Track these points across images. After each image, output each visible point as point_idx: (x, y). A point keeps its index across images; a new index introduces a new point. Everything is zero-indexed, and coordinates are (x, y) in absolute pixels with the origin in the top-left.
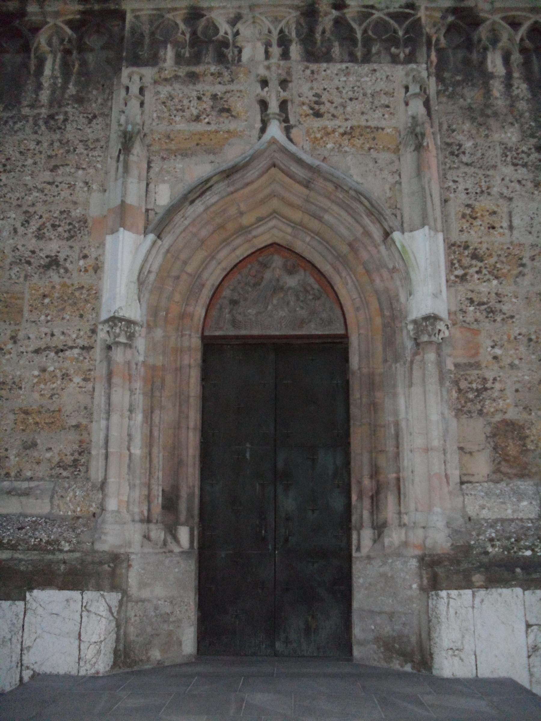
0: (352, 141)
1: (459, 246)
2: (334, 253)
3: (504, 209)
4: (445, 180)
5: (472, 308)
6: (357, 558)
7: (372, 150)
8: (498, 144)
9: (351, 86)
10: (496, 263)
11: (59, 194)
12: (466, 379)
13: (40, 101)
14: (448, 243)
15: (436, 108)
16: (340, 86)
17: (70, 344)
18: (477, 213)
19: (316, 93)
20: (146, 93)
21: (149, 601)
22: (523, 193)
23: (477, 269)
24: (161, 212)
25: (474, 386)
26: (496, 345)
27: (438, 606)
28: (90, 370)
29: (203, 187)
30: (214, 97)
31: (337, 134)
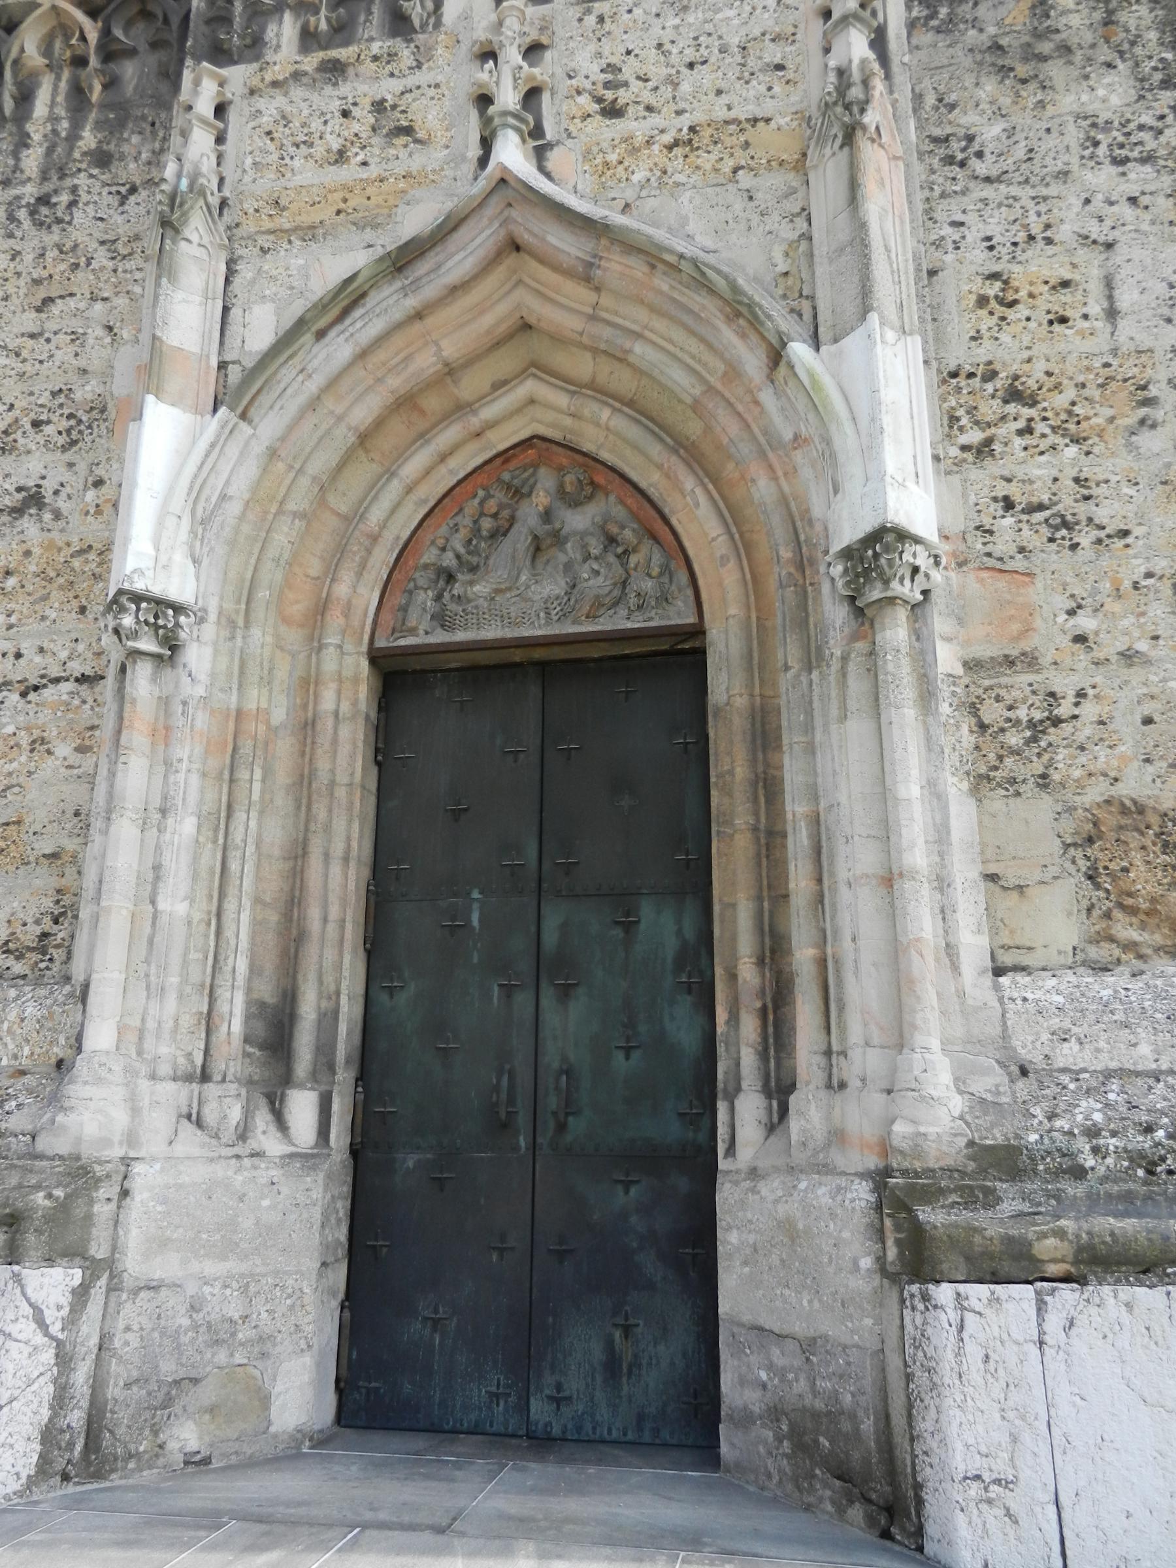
0: (692, 158)
1: (971, 375)
2: (669, 440)
3: (1091, 268)
4: (930, 224)
5: (1009, 521)
6: (728, 1172)
7: (741, 172)
8: (1071, 119)
9: (692, 35)
10: (1073, 404)
11: (51, 356)
12: (998, 699)
13: (22, 171)
14: (939, 371)
15: (906, 59)
16: (666, 41)
17: (55, 672)
18: (1017, 291)
19: (609, 65)
20: (232, 115)
21: (176, 1286)
22: (1145, 227)
23: (1021, 424)
24: (249, 363)
25: (1022, 713)
26: (1080, 607)
27: (929, 1331)
28: (92, 728)
29: (348, 298)
30: (379, 106)
31: (656, 148)
